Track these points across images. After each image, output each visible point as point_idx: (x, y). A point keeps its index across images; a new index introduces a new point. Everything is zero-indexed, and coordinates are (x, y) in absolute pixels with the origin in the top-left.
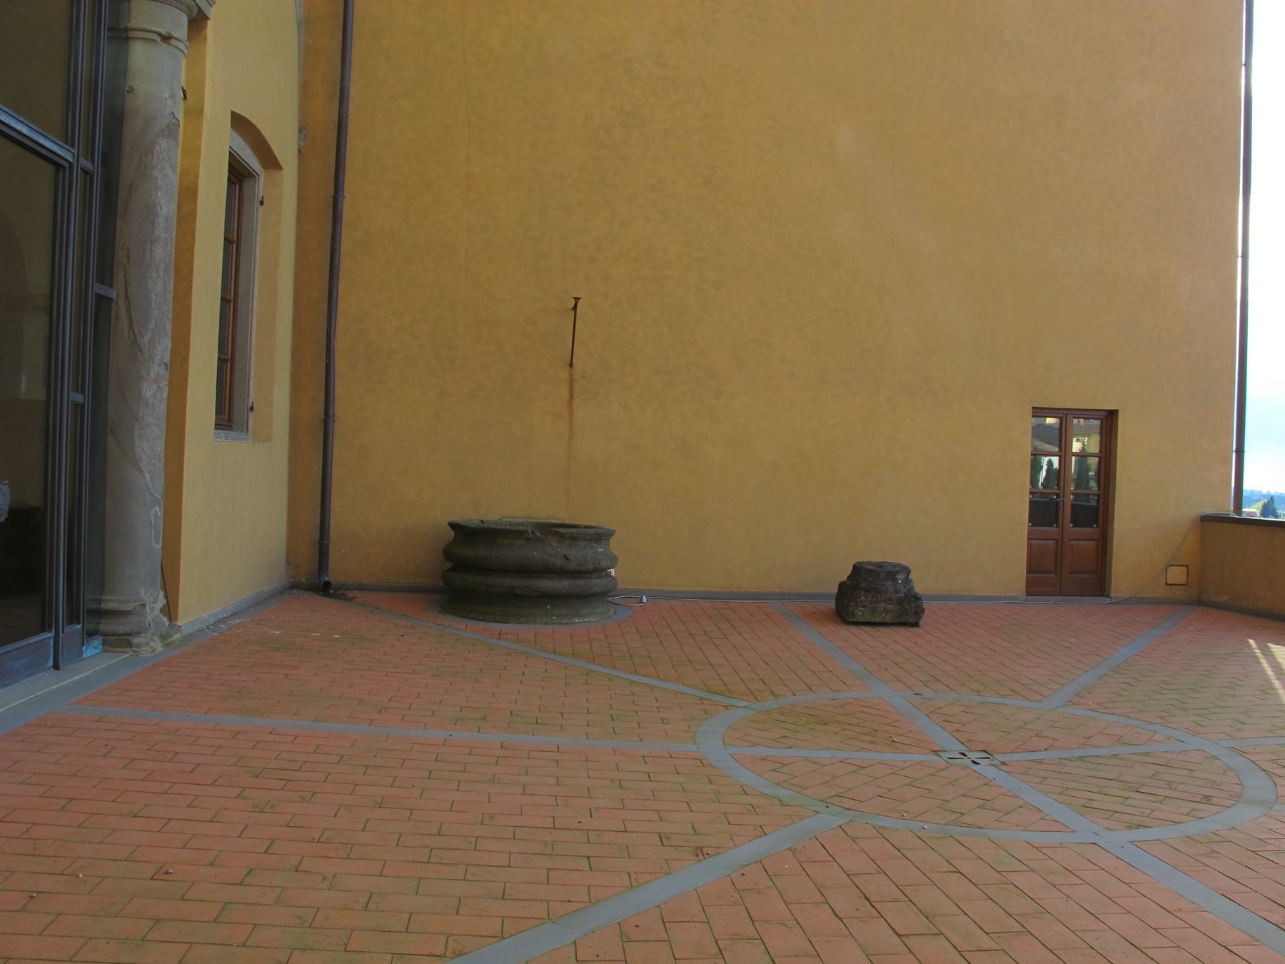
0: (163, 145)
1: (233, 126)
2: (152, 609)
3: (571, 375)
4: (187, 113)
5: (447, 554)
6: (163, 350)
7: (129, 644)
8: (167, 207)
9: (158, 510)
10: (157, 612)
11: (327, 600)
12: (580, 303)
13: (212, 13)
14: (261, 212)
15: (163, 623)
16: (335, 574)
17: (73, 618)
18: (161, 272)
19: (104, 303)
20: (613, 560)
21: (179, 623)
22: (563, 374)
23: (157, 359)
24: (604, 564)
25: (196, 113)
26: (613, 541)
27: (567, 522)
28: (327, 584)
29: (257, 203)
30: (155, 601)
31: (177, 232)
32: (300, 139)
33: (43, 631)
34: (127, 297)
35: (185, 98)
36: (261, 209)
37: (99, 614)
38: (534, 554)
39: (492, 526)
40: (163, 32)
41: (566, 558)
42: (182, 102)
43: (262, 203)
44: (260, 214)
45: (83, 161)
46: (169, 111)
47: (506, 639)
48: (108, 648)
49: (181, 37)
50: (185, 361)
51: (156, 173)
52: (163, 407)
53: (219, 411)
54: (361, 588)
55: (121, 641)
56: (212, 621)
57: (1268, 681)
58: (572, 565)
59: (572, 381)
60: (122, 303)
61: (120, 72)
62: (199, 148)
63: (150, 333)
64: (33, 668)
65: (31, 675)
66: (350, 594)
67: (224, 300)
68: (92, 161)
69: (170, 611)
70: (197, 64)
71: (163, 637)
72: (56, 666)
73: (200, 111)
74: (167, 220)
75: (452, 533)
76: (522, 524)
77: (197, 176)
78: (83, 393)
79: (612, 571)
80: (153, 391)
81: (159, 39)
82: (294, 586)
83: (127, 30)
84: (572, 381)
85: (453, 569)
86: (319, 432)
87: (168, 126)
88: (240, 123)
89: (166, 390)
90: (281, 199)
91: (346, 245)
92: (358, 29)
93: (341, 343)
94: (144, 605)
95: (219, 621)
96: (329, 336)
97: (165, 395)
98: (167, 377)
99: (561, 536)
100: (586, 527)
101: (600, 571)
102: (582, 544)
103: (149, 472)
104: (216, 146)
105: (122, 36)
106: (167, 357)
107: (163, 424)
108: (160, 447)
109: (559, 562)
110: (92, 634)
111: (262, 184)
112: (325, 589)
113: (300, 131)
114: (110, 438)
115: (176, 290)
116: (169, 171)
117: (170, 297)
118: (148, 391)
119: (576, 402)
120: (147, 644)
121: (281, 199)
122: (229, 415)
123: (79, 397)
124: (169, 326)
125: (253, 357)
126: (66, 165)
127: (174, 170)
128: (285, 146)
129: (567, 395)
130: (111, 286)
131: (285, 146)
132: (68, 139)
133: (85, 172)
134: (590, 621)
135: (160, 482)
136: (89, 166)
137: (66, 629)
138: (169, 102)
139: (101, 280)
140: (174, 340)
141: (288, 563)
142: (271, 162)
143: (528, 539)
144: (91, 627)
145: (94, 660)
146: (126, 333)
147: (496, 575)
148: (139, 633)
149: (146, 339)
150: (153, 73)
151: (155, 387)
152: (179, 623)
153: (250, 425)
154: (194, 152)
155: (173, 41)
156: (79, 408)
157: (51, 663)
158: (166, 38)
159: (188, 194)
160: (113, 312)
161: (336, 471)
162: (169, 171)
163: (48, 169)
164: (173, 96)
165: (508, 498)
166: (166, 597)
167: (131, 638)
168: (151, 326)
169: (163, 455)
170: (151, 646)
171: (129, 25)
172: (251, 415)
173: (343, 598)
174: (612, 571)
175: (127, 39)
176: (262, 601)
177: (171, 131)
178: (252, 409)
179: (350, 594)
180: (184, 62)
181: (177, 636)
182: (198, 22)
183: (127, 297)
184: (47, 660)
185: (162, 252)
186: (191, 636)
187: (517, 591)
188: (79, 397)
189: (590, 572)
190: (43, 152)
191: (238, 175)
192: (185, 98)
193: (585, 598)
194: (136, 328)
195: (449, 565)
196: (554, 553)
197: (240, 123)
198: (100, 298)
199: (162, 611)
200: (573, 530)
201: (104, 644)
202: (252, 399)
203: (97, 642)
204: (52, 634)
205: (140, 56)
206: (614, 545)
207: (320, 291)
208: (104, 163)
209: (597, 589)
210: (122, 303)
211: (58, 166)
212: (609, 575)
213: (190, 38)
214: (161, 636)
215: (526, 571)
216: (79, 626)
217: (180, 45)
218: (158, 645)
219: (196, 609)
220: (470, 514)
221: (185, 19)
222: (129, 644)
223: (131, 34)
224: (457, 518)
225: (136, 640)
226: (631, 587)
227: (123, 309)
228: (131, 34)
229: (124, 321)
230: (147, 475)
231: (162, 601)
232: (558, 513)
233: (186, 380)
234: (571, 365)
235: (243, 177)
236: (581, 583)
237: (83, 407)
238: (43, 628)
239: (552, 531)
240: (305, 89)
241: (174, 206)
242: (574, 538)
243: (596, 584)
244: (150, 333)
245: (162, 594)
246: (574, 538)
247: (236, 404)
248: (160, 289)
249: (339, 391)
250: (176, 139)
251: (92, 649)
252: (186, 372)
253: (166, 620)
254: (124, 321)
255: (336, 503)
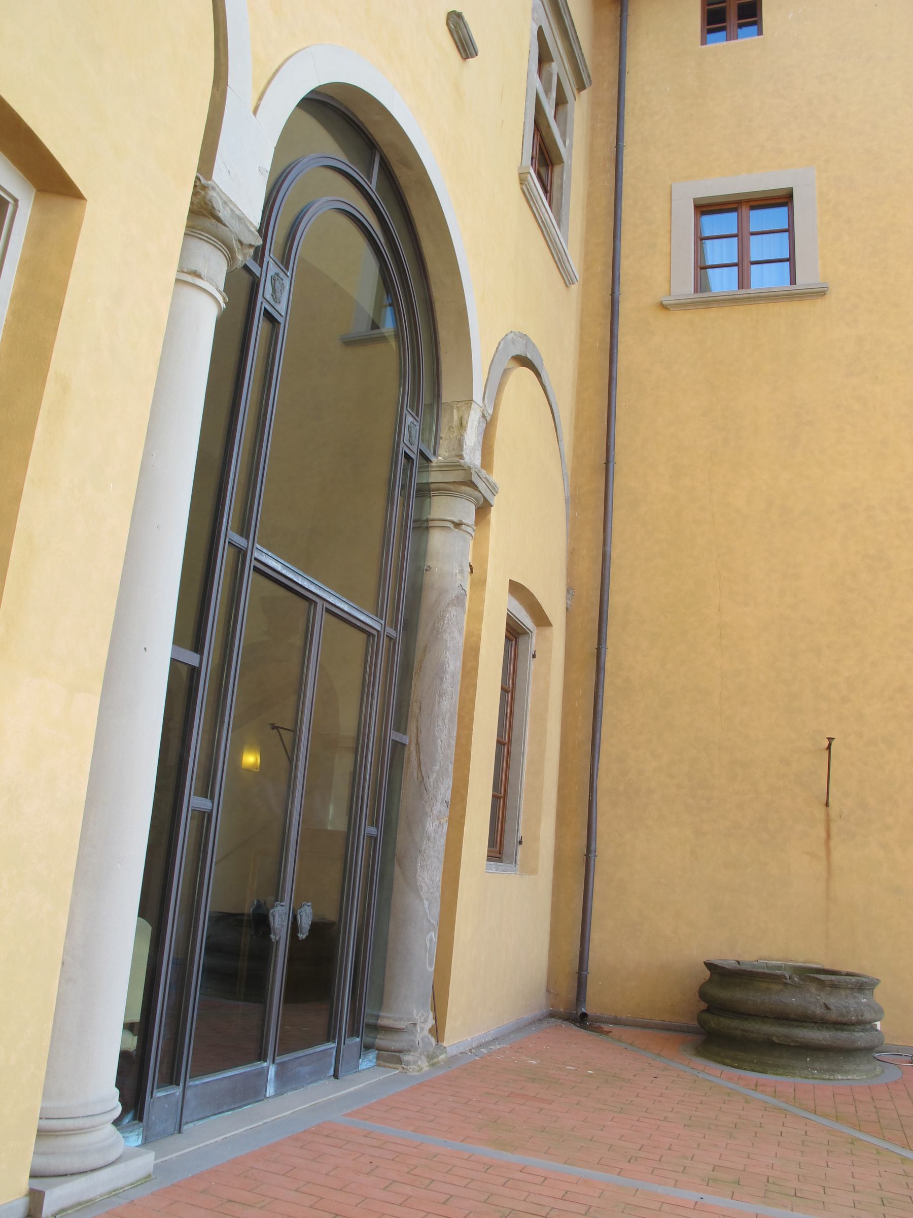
0: (453, 612)
1: (510, 592)
2: (422, 1029)
3: (828, 815)
4: (473, 584)
5: (703, 994)
6: (445, 790)
7: (399, 1061)
8: (453, 665)
9: (433, 935)
10: (426, 1032)
11: (583, 1032)
12: (833, 743)
13: (495, 501)
14: (533, 664)
15: (430, 1043)
16: (591, 1008)
17: (354, 1031)
18: (447, 721)
19: (399, 748)
20: (879, 1013)
21: (445, 1044)
22: (820, 813)
23: (440, 798)
24: (868, 1016)
25: (480, 583)
26: (877, 990)
27: (827, 967)
28: (584, 1015)
29: (530, 656)
30: (425, 1021)
31: (462, 685)
32: (567, 599)
33: (328, 1041)
34: (417, 743)
35: (472, 571)
36: (533, 661)
37: (376, 1028)
38: (793, 1000)
39: (748, 968)
40: (456, 520)
41: (827, 1007)
42: (469, 575)
43: (534, 656)
44: (532, 667)
45: (388, 629)
46: (458, 584)
47: (763, 1092)
48: (382, 1063)
49: (470, 523)
50: (464, 799)
51: (446, 636)
52: (443, 841)
53: (492, 842)
54: (616, 1022)
55: (392, 1057)
56: (475, 1044)
57: (348, 1093)
58: (833, 1016)
59: (828, 820)
60: (413, 748)
61: (420, 554)
62: (481, 613)
63: (435, 775)
64: (317, 1075)
65: (315, 1081)
66: (606, 1027)
67: (500, 743)
68: (396, 629)
69: (437, 1032)
70: (481, 544)
71: (430, 1057)
72: (336, 1076)
73: (484, 582)
74: (453, 677)
75: (708, 973)
76: (779, 967)
77: (479, 637)
78: (377, 827)
79: (878, 1023)
80: (435, 827)
81: (452, 526)
82: (552, 1015)
83: (427, 521)
84: (828, 820)
85: (708, 1010)
86: (581, 864)
87: (457, 597)
88: (516, 589)
89: (446, 826)
90: (551, 653)
91: (608, 692)
92: (617, 501)
93: (603, 783)
94: (415, 1024)
95: (481, 1046)
96: (592, 775)
97: (445, 830)
98: (447, 813)
99: (821, 982)
100: (848, 974)
101: (864, 1024)
102: (843, 992)
103: (427, 900)
104: (497, 606)
105: (423, 526)
106: (448, 797)
107: (442, 856)
108: (438, 877)
109: (819, 1011)
110: (368, 1047)
111: (534, 642)
112: (582, 1020)
113: (568, 591)
114: (397, 868)
115: (458, 736)
116: (456, 634)
117: (453, 742)
118: (431, 826)
119: (833, 843)
120: (415, 1062)
121: (551, 653)
122: (499, 848)
123: (373, 831)
124: (451, 768)
125: (523, 795)
126: (375, 633)
127: (460, 632)
128: (555, 606)
129: (823, 834)
130: (405, 733)
131: (555, 606)
132: (378, 613)
133: (390, 638)
134: (854, 1078)
135: (436, 911)
136: (392, 633)
137: (347, 1040)
138: (459, 576)
139: (398, 730)
140: (455, 780)
141: (548, 991)
142: (542, 620)
143: (786, 984)
144: (368, 1040)
145: (368, 1074)
146: (415, 775)
147: (749, 1019)
148: (409, 1051)
149: (431, 780)
150: (447, 553)
151: (437, 823)
152: (445, 1044)
153: (518, 858)
154: (477, 616)
155: (463, 527)
156: (373, 839)
157: (332, 1072)
158: (458, 525)
159: (472, 652)
160: (406, 756)
161: (597, 905)
162: (456, 634)
163: (365, 636)
164: (462, 571)
165: (768, 939)
166: (435, 1018)
167: (401, 1055)
168: (437, 768)
169: (440, 884)
170: (418, 1065)
171: (430, 517)
172: (520, 848)
173: (599, 1031)
174: (878, 1025)
175: (428, 528)
176: (521, 1027)
177: (459, 600)
178: (520, 843)
179: (606, 1027)
180: (471, 542)
181: (442, 1057)
182: (483, 509)
183: (417, 743)
184: (329, 1069)
185: (448, 704)
186: (454, 1058)
187: (774, 1039)
188: (373, 831)
189: (853, 1024)
190: (359, 624)
191: (514, 633)
192: (472, 571)
193: (848, 1052)
194: (423, 769)
195: (703, 1005)
196: (812, 1000)
197: (516, 589)
198: (395, 743)
199: (430, 1031)
200: (833, 978)
201: (378, 1058)
202: (521, 833)
203: (372, 1055)
204: (334, 1045)
205: (437, 540)
206: (879, 995)
207: (583, 734)
208: (405, 629)
209: (860, 1044)
210: (413, 748)
211: (369, 634)
212: (874, 1029)
213: (477, 522)
214: (428, 1056)
215: (783, 1017)
216: (358, 1039)
217: (470, 530)
218: (424, 1064)
219: (461, 1033)
220: (728, 954)
221: (473, 508)
222: (399, 1061)
223: (431, 524)
224: (713, 958)
225: (406, 1058)
226: (900, 1043)
227: (414, 753)
228: (431, 524)
229: (414, 763)
230: (426, 903)
231: (431, 1022)
232: (819, 958)
233: (463, 817)
234: (827, 805)
235: (519, 634)
236: (842, 1036)
237: (376, 839)
238: (328, 1039)
239: (812, 976)
240: (572, 554)
241: (459, 664)
242: (835, 986)
243: (860, 1038)
244: (435, 775)
245: (431, 1015)
246: (835, 986)
247: (507, 838)
248: (444, 736)
249: (601, 827)
250: (463, 606)
251: (368, 1062)
252: (464, 809)
253: (433, 1040)
254: (414, 763)
255: (595, 936)
